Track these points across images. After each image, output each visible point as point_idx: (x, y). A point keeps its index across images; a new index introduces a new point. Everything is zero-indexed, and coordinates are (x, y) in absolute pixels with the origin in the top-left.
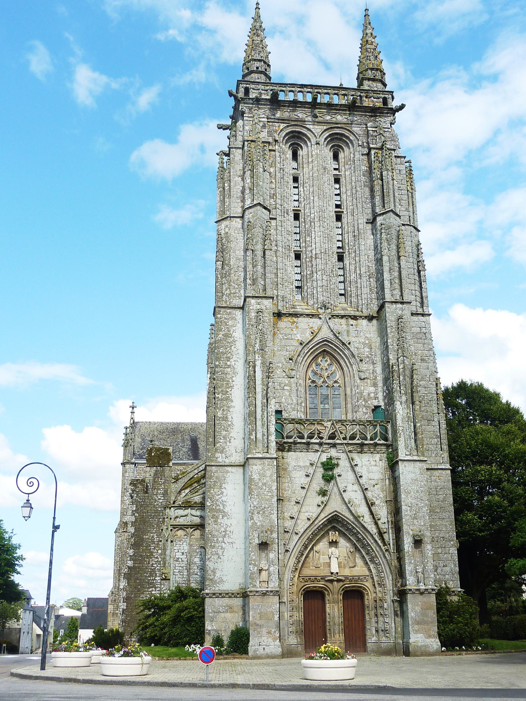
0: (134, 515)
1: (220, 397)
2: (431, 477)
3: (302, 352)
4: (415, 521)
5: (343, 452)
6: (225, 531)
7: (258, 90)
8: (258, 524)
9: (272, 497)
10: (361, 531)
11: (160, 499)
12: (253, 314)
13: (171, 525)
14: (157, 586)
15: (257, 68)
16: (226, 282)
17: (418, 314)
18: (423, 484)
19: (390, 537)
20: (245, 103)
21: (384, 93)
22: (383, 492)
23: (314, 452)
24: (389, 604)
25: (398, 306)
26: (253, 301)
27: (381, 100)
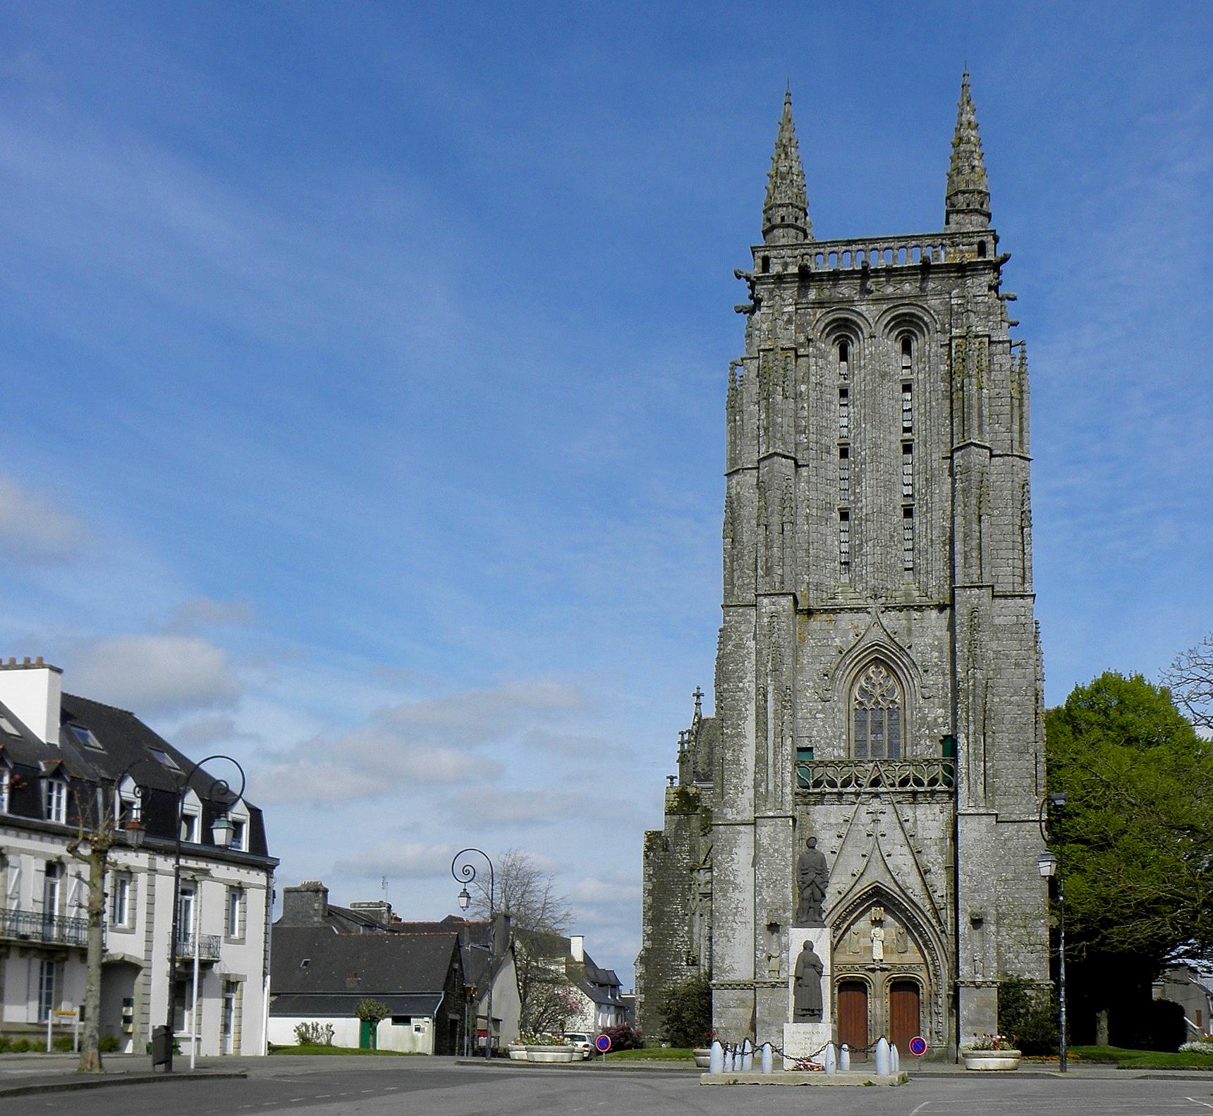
0: (651, 880)
1: (729, 733)
2: (1018, 832)
3: (842, 664)
4: (976, 894)
5: (889, 804)
6: (737, 908)
7: (781, 258)
8: (767, 901)
9: (786, 866)
10: (910, 906)
11: (685, 859)
12: (766, 620)
13: (700, 894)
14: (683, 973)
15: (783, 218)
16: (738, 568)
17: (1015, 596)
18: (989, 846)
19: (947, 914)
20: (762, 284)
21: (981, 234)
22: (942, 855)
23: (849, 804)
24: (943, 1001)
25: (973, 592)
26: (766, 601)
27: (976, 247)
